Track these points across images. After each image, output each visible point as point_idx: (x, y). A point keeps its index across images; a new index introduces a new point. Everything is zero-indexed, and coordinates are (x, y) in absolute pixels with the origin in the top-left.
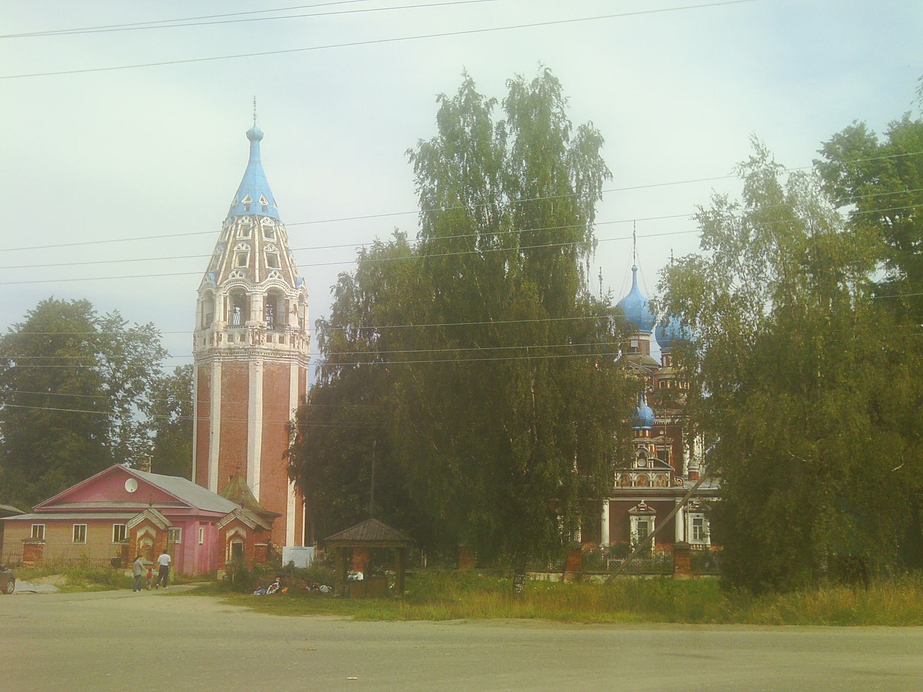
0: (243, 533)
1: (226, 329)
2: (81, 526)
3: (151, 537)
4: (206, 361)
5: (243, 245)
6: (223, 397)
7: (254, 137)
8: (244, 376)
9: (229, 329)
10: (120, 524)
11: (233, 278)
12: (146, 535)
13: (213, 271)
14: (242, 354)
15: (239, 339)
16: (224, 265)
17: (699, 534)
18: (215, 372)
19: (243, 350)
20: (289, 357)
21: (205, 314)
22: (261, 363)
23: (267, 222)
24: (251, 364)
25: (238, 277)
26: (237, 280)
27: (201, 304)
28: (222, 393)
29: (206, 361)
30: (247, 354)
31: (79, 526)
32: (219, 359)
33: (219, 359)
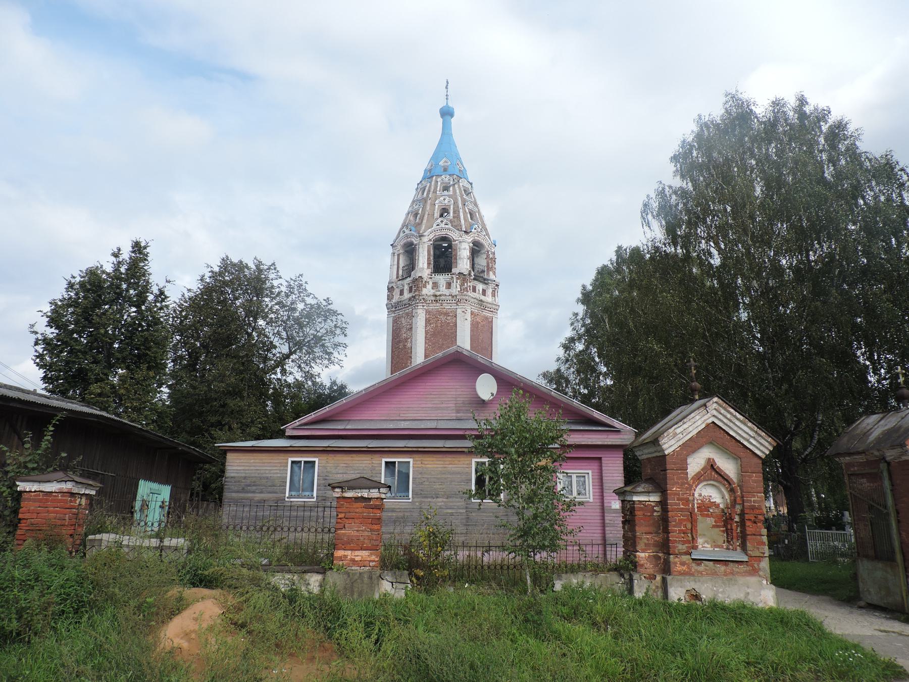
0: (728, 467)
1: (430, 276)
2: (305, 462)
3: (723, 477)
4: (404, 311)
5: (444, 199)
6: (427, 345)
7: (447, 113)
8: (452, 324)
9: (433, 276)
10: (303, 459)
11: (438, 227)
12: (712, 471)
13: (416, 217)
14: (448, 302)
15: (445, 287)
16: (426, 216)
17: (313, 491)
18: (418, 320)
19: (450, 297)
20: (491, 310)
21: (401, 266)
22: (469, 311)
23: (464, 183)
24: (459, 311)
25: (443, 225)
26: (442, 229)
27: (396, 257)
28: (426, 342)
29: (404, 311)
30: (454, 301)
31: (300, 462)
32: (423, 306)
33: (423, 306)
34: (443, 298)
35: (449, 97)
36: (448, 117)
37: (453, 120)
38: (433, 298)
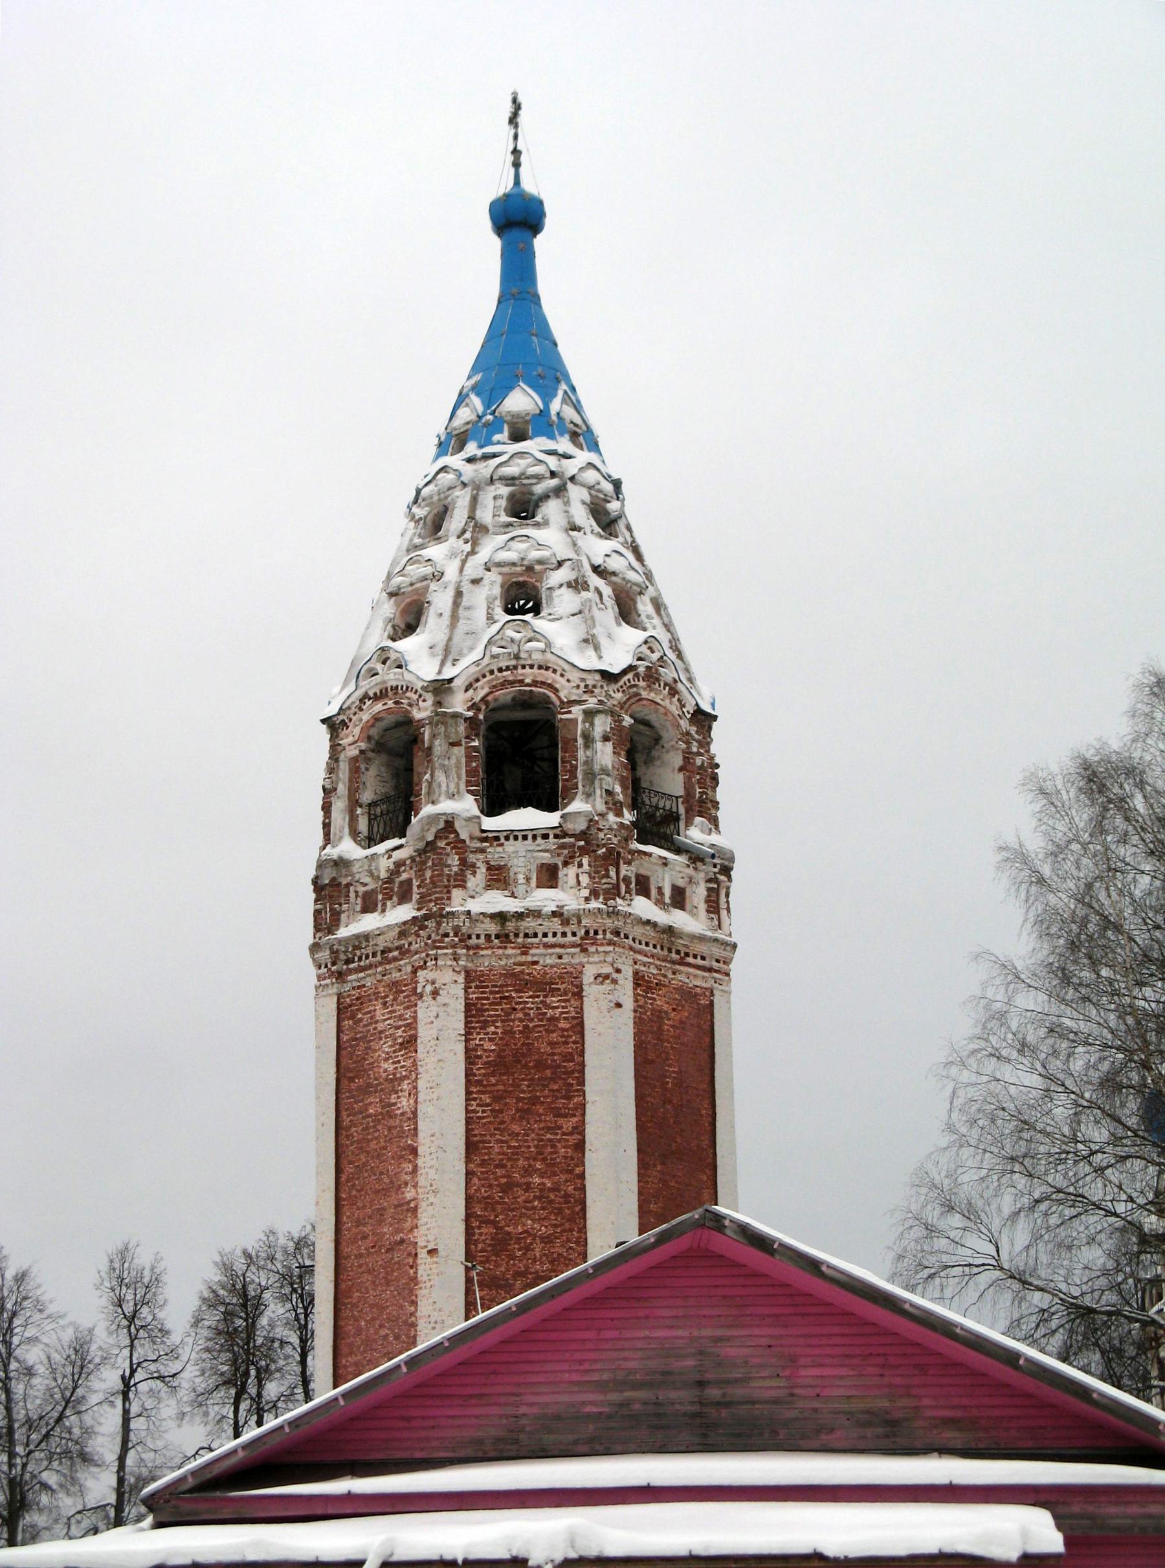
14: (550, 939)
19: (556, 925)
34: (529, 924)
35: (523, 159)
36: (516, 234)
37: (541, 243)
38: (492, 928)
